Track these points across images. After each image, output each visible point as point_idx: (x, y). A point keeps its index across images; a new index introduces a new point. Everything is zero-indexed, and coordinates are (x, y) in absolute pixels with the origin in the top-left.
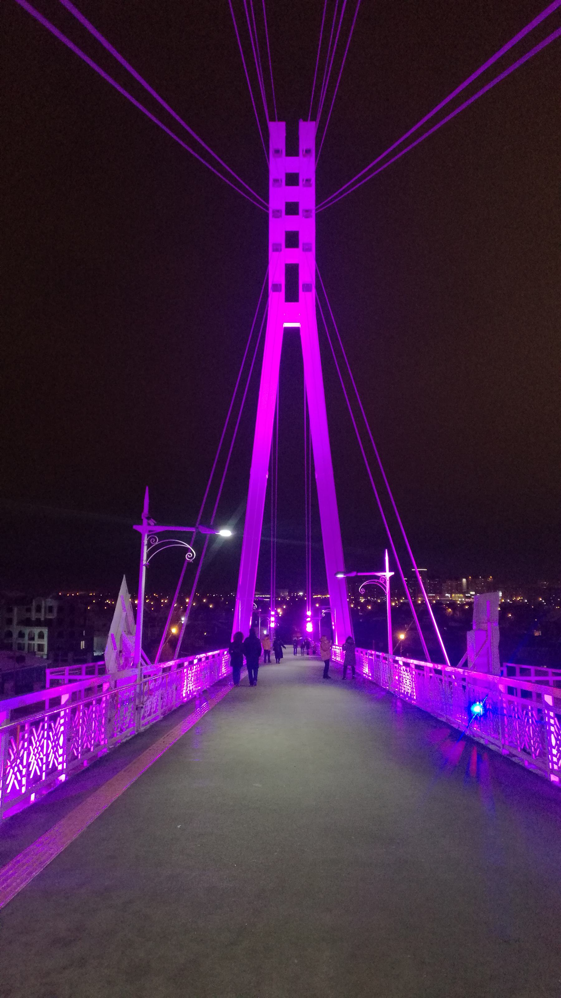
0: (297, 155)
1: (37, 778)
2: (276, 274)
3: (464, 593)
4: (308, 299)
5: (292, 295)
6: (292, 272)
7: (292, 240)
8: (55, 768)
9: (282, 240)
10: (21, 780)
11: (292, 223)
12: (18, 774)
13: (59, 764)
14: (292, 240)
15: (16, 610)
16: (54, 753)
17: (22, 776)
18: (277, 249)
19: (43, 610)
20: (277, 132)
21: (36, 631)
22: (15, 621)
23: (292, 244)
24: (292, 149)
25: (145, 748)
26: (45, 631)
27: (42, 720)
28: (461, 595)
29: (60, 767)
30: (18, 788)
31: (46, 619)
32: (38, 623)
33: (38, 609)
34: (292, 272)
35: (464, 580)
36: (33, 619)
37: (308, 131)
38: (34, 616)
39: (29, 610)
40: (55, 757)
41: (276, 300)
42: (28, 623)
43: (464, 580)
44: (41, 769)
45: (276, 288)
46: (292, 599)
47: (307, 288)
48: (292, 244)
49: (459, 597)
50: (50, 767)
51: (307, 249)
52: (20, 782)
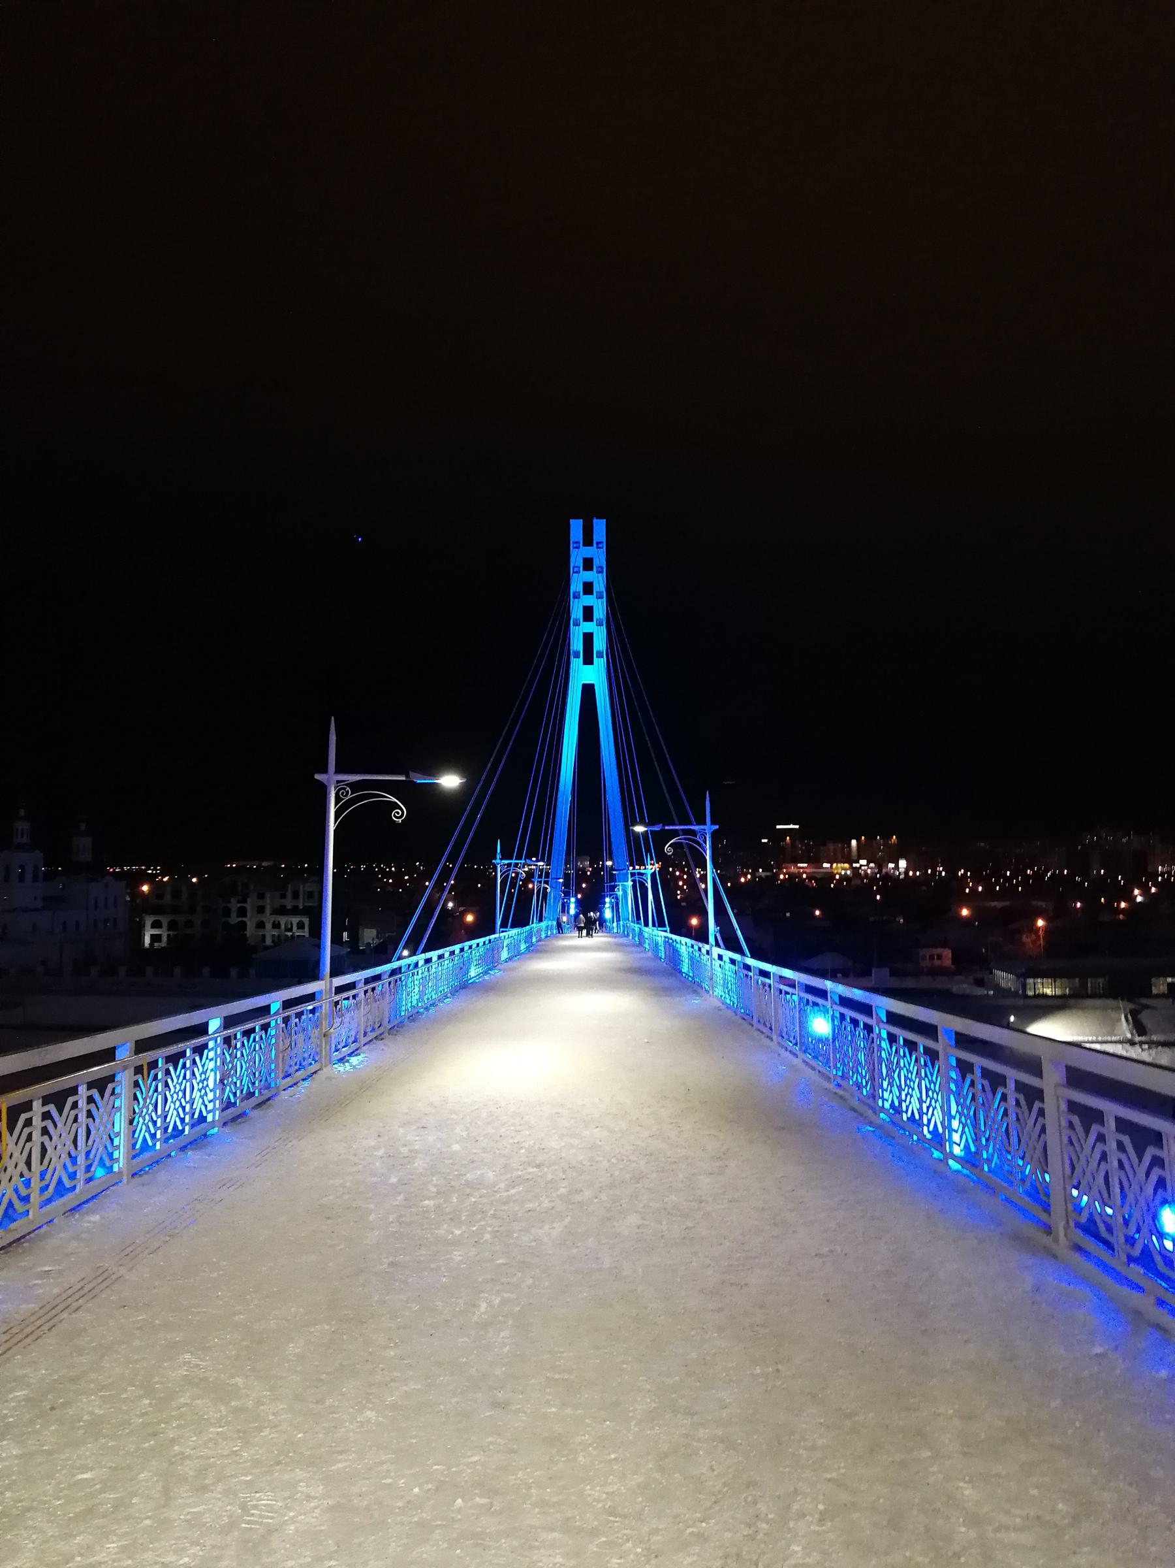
0: (592, 545)
1: (177, 1133)
2: (577, 644)
3: (851, 862)
4: (600, 663)
5: (588, 660)
6: (588, 638)
7: (588, 564)
8: (202, 1119)
9: (580, 588)
10: (155, 1134)
11: (588, 600)
12: (150, 1124)
13: (208, 1112)
14: (588, 588)
15: (268, 896)
16: (202, 1097)
17: (156, 1129)
18: (576, 596)
19: (301, 897)
20: (576, 527)
21: (295, 920)
22: (268, 910)
23: (589, 619)
24: (588, 541)
25: (46, 1236)
26: (306, 920)
27: (253, 1030)
28: (847, 865)
29: (210, 1118)
30: (150, 1143)
31: (304, 907)
32: (295, 911)
33: (296, 895)
34: (588, 638)
35: (854, 843)
36: (289, 907)
37: (600, 527)
38: (289, 903)
39: (283, 896)
40: (203, 1103)
41: (577, 663)
42: (282, 911)
43: (854, 843)
44: (182, 1120)
45: (577, 656)
46: (596, 872)
47: (600, 655)
48: (589, 619)
49: (843, 869)
50: (196, 1116)
51: (599, 597)
52: (153, 1136)
